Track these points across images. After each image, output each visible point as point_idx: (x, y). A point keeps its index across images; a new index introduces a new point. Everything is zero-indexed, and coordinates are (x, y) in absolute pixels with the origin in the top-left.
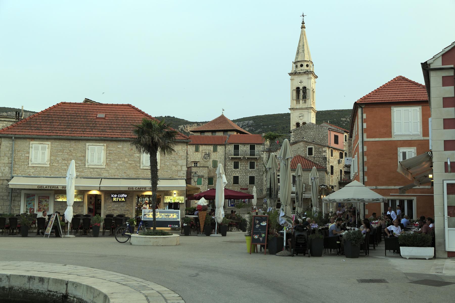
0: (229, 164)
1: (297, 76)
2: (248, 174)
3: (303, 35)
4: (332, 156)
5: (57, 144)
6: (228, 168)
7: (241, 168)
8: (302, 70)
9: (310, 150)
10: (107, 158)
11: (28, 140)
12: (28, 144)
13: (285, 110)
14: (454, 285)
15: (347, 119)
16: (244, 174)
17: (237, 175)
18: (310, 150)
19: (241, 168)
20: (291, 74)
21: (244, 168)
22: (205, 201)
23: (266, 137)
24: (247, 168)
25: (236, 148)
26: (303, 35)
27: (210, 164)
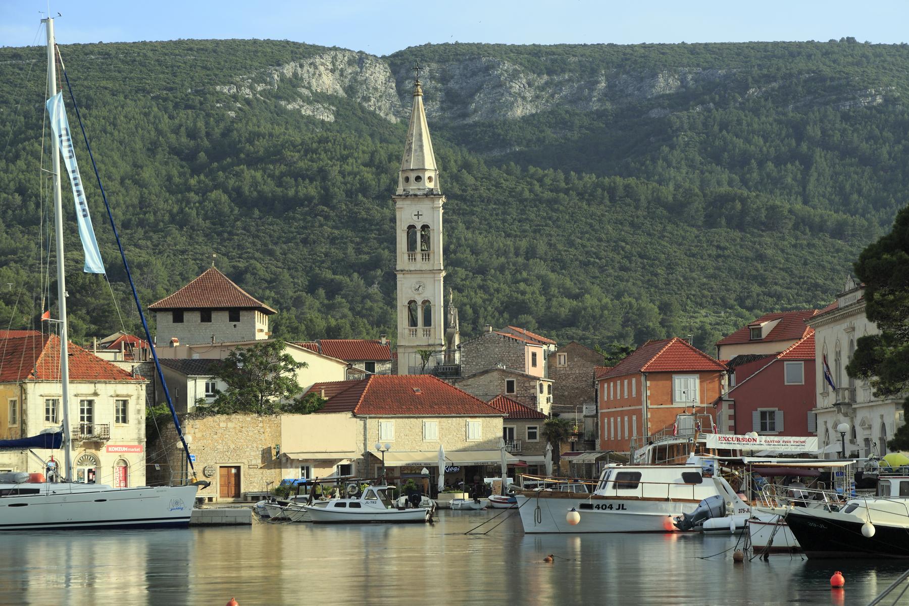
1: (408, 202)
8: (419, 189)
9: (510, 385)
14: (6, 436)
15: (239, 87)
18: (510, 385)
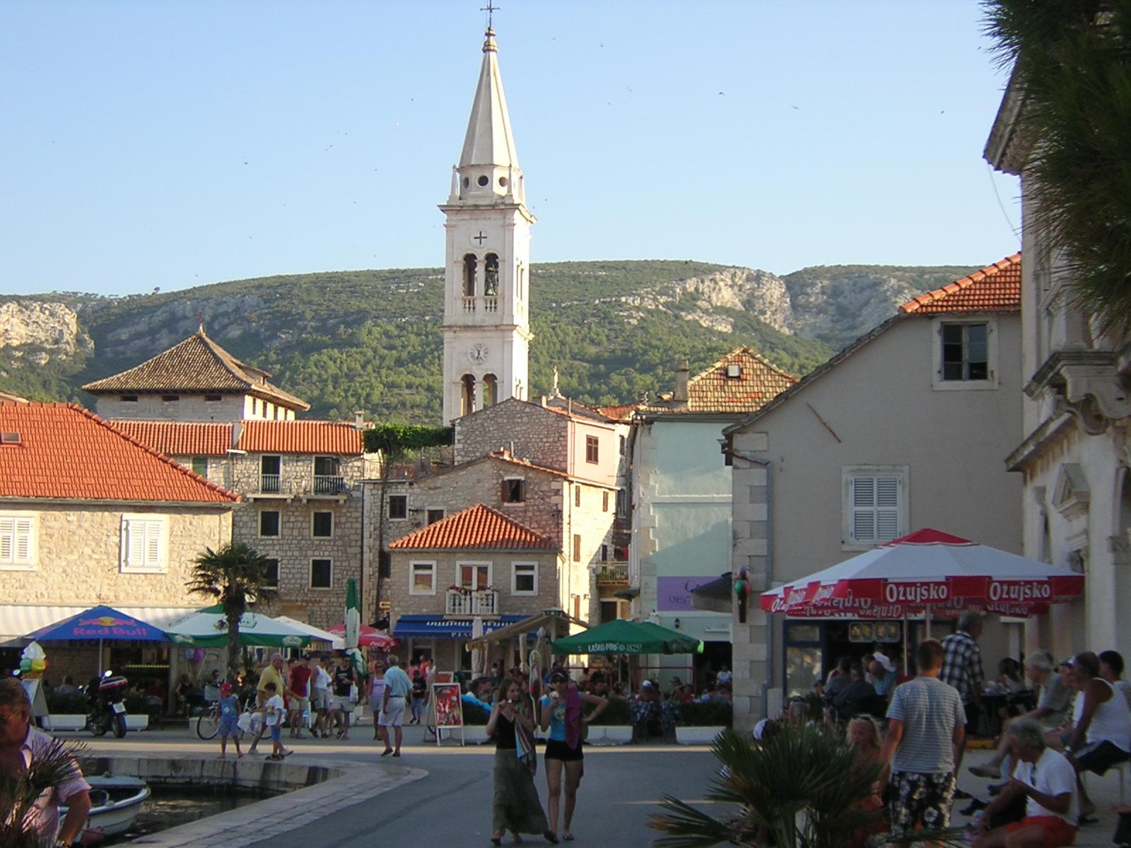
0: (245, 519)
2: (310, 553)
4: (578, 504)
6: (243, 531)
7: (287, 532)
10: (41, 547)
16: (296, 553)
19: (287, 532)
20: (444, 209)
21: (296, 532)
22: (775, 689)
23: (373, 441)
24: (306, 532)
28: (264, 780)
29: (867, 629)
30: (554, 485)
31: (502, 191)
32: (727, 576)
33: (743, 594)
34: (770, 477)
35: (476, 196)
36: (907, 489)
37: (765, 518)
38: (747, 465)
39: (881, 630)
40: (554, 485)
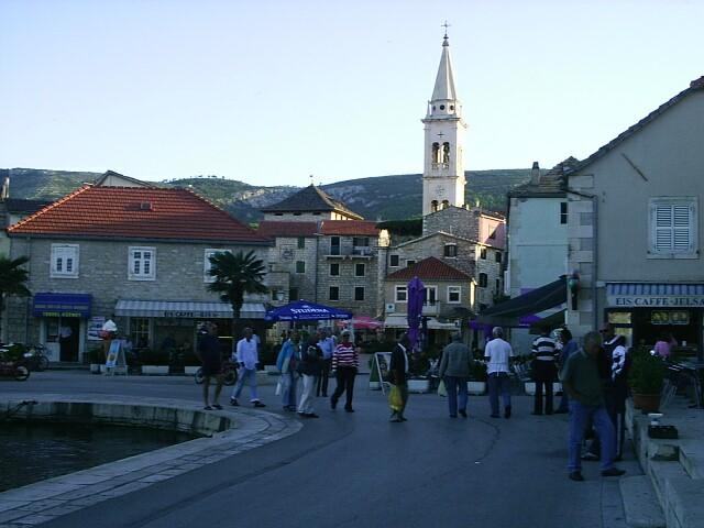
3: (444, 56)
5: (88, 246)
11: (48, 241)
12: (47, 246)
13: (420, 170)
17: (336, 285)
25: (335, 242)
26: (444, 56)
27: (293, 266)
28: (193, 426)
29: (665, 316)
30: (471, 248)
31: (452, 112)
32: (563, 277)
33: (575, 289)
34: (596, 207)
35: (441, 115)
36: (696, 215)
37: (591, 235)
38: (578, 198)
39: (676, 316)
40: (471, 248)
